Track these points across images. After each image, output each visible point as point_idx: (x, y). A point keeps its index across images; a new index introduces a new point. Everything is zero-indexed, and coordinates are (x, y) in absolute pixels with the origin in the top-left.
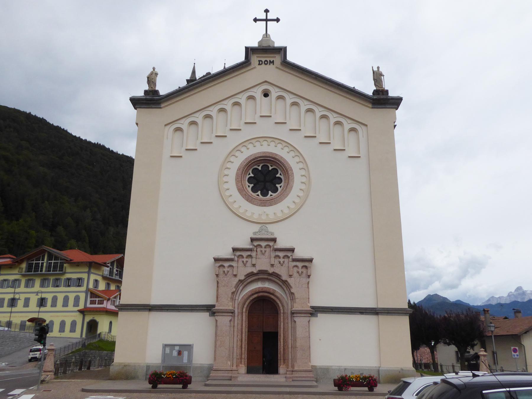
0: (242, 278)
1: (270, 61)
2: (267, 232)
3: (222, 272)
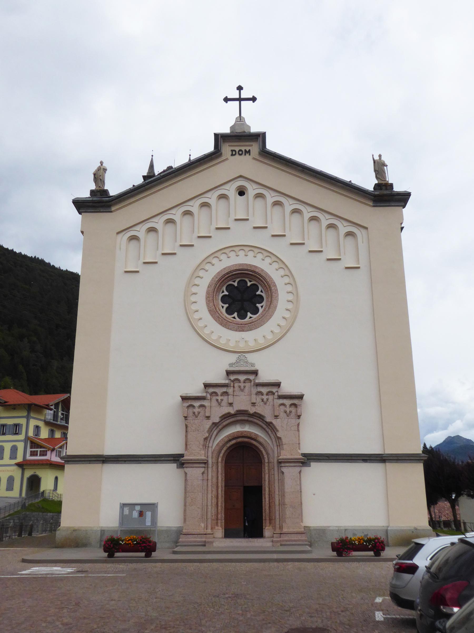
1: (245, 150)
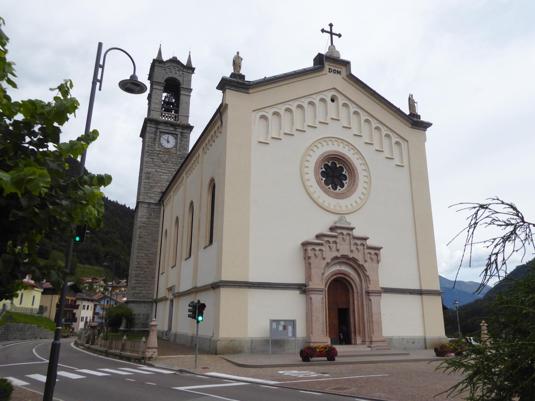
0: (329, 261)
2: (346, 221)
3: (313, 255)
